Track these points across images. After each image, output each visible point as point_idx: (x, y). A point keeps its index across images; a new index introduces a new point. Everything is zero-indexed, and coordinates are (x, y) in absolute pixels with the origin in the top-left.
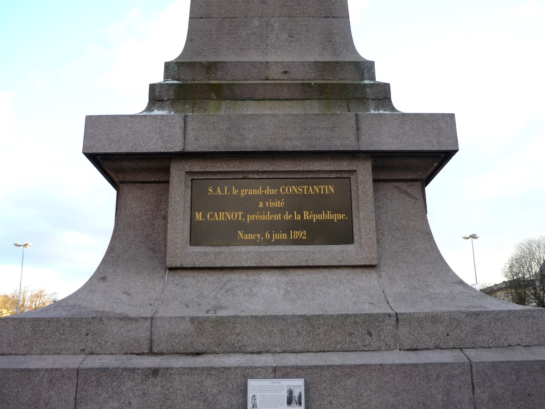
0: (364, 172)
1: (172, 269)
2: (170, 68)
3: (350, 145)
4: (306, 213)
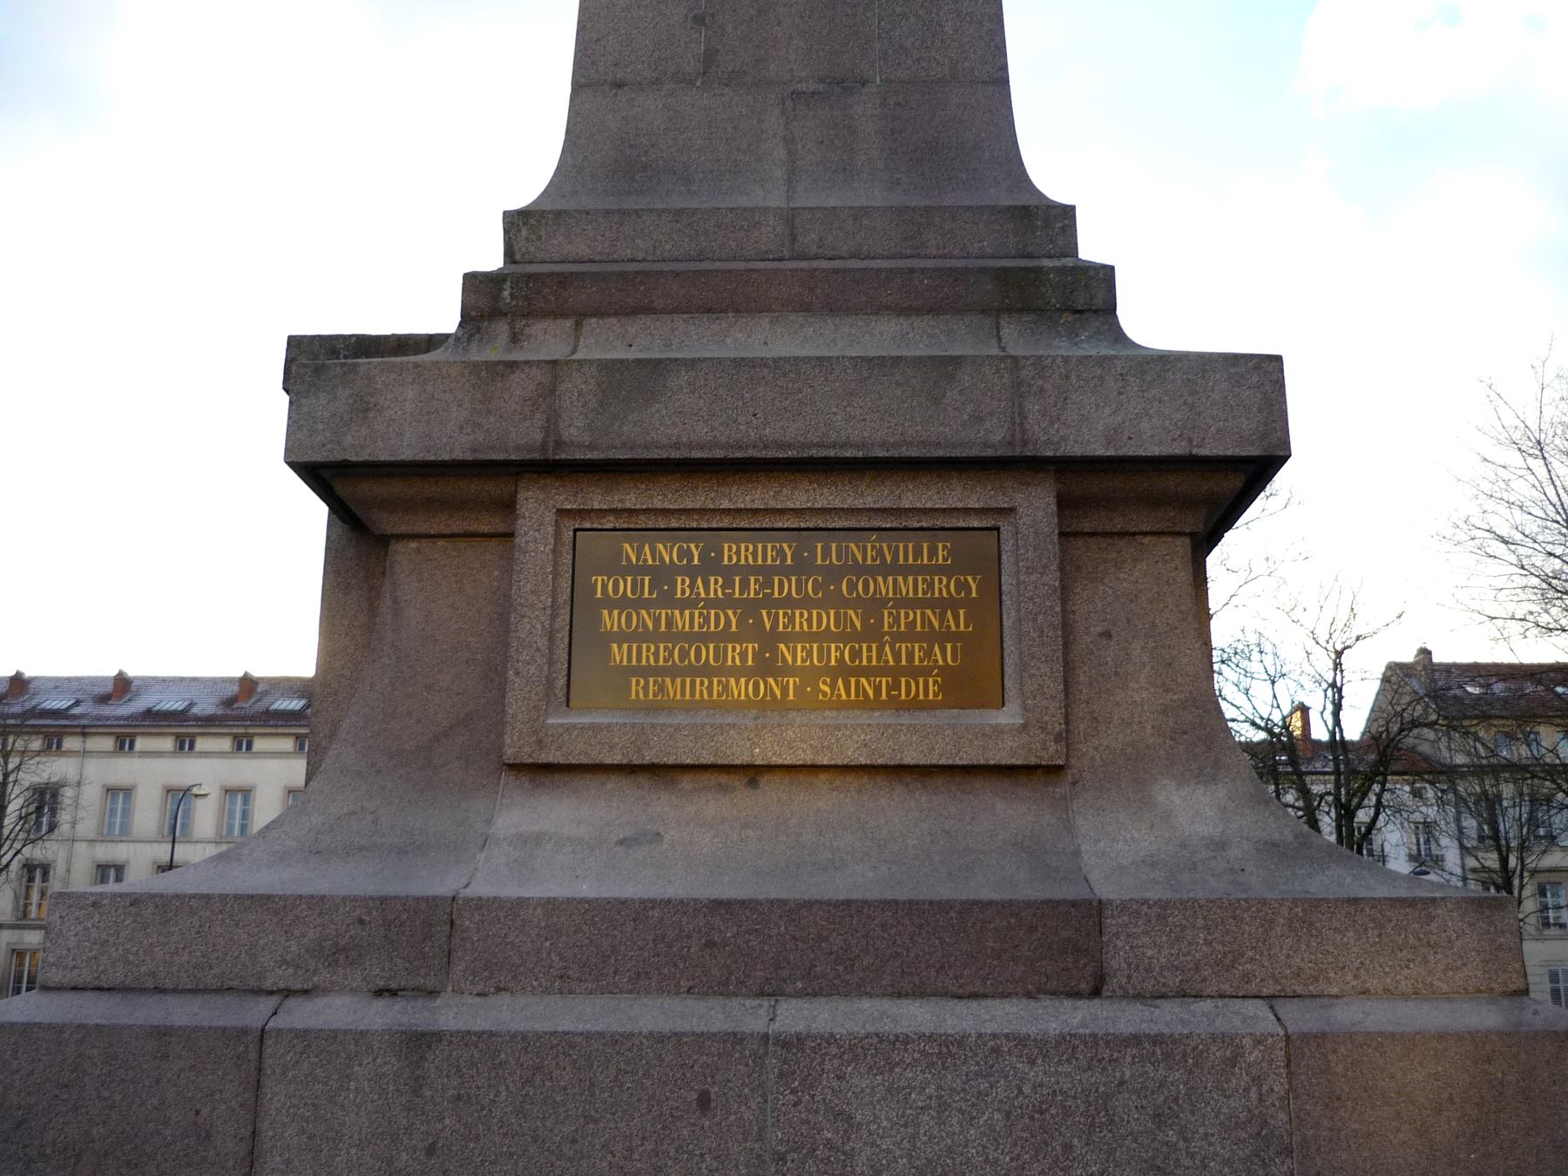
0: (1036, 506)
1: (518, 768)
2: (516, 223)
3: (992, 437)
4: (683, 582)
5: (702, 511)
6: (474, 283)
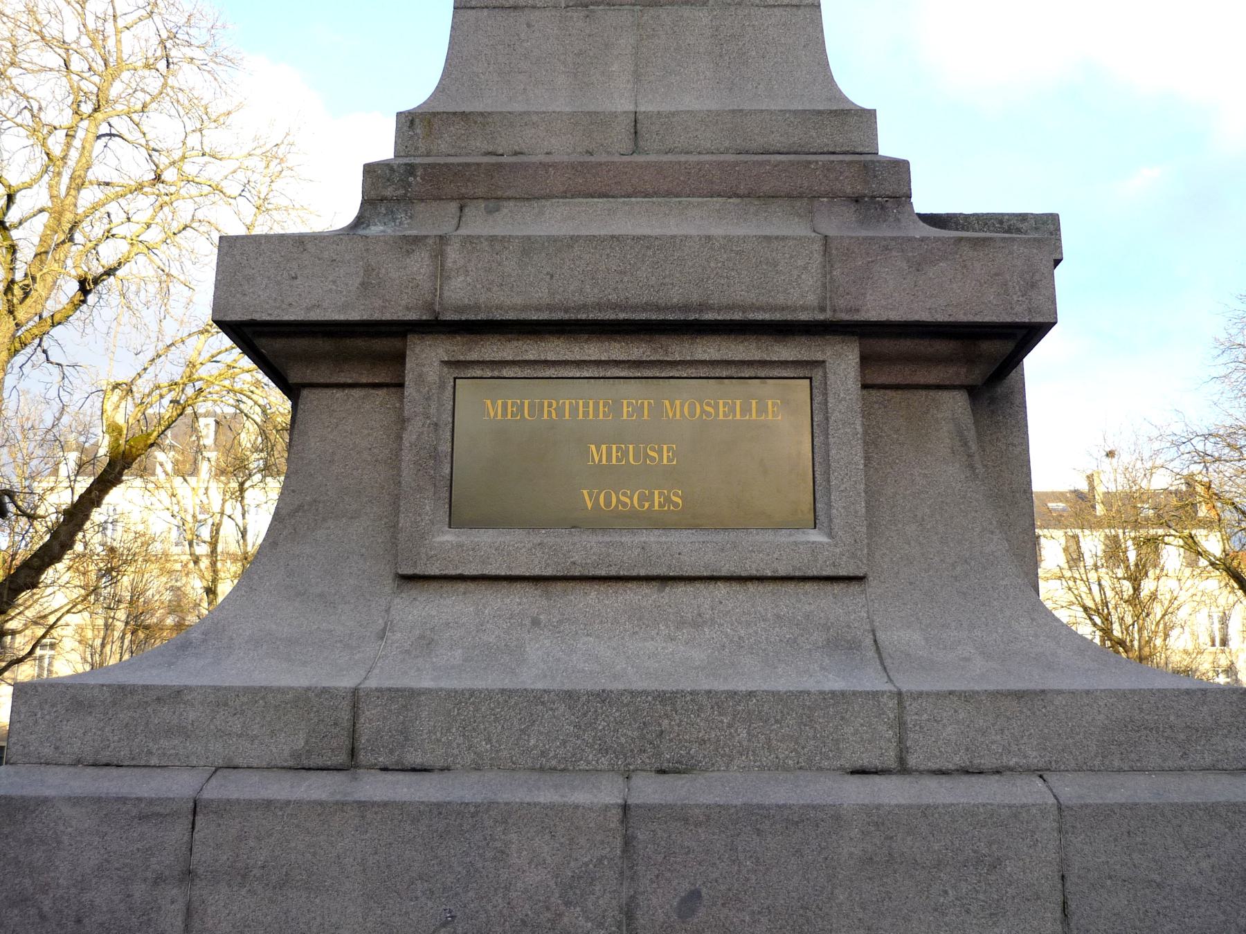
2: (409, 122)
5: (598, 363)
6: (372, 171)
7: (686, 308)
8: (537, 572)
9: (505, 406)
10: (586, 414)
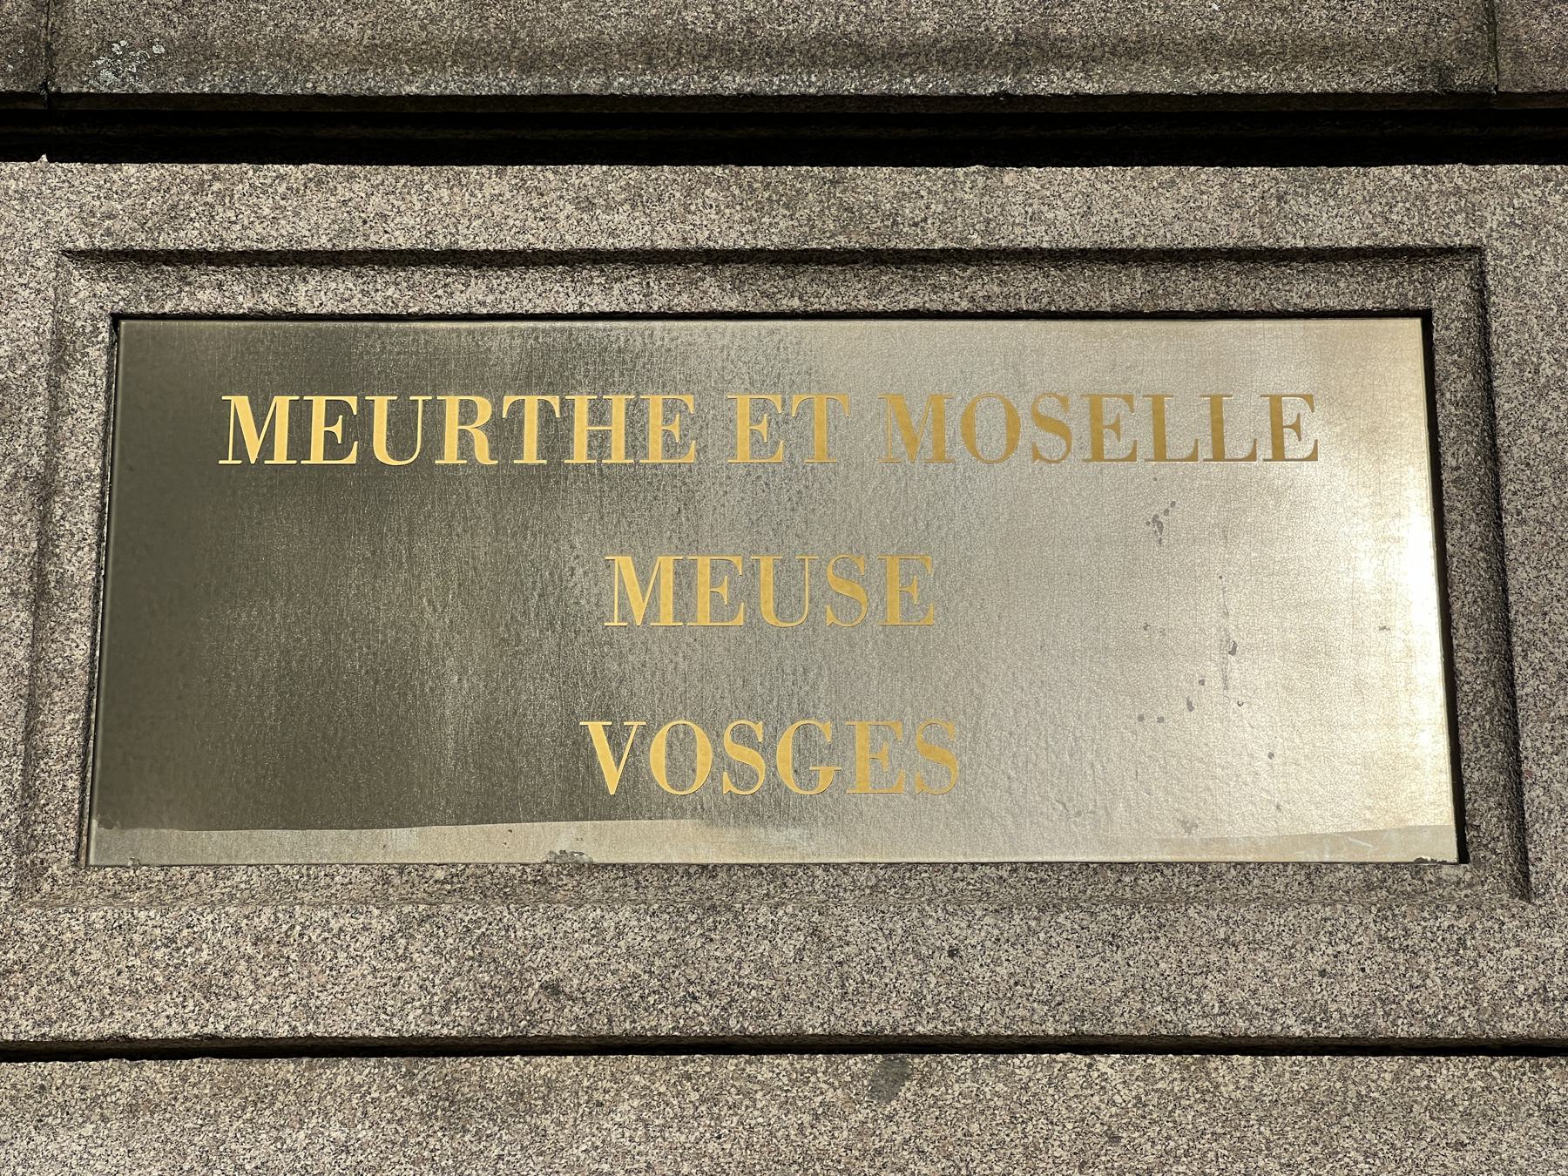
7: (967, 51)
8: (413, 1024)
9: (685, 576)
10: (599, 443)
